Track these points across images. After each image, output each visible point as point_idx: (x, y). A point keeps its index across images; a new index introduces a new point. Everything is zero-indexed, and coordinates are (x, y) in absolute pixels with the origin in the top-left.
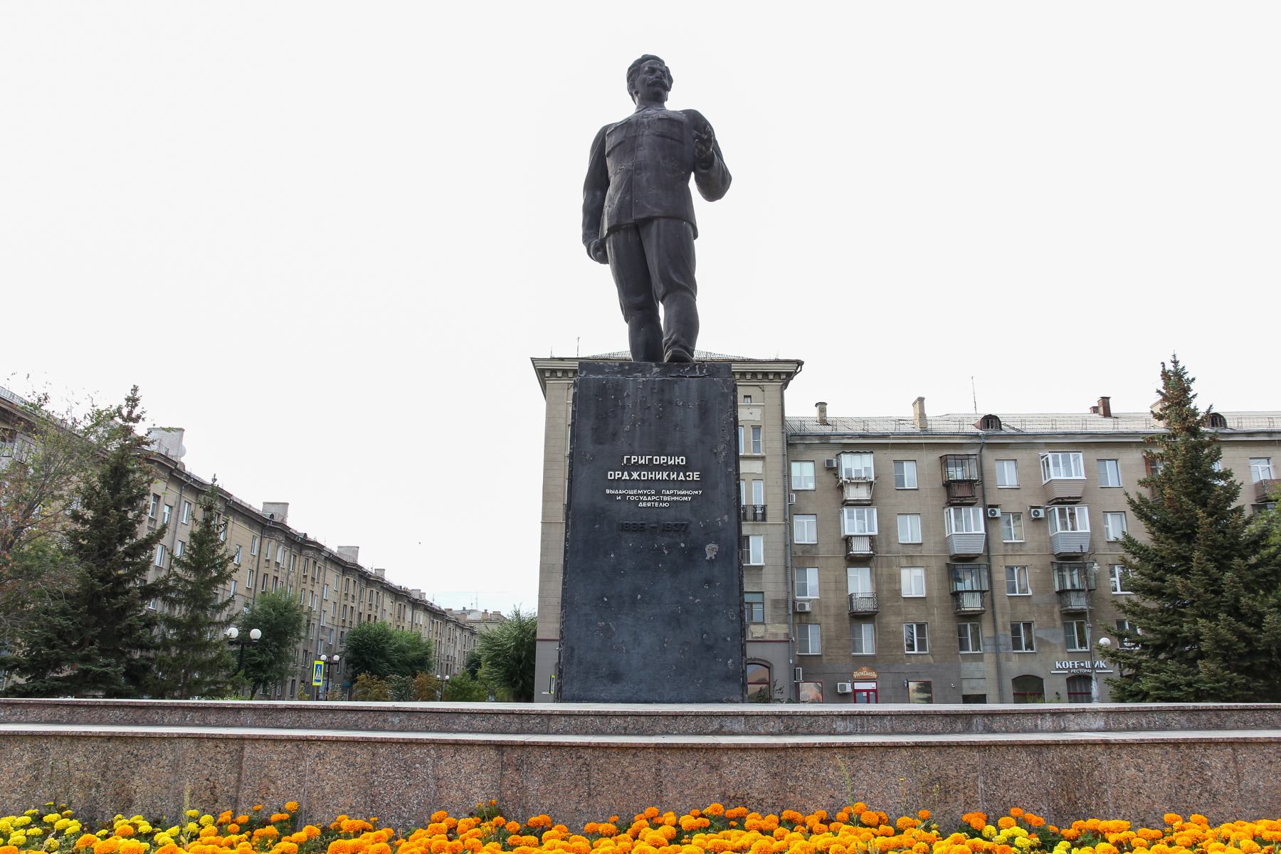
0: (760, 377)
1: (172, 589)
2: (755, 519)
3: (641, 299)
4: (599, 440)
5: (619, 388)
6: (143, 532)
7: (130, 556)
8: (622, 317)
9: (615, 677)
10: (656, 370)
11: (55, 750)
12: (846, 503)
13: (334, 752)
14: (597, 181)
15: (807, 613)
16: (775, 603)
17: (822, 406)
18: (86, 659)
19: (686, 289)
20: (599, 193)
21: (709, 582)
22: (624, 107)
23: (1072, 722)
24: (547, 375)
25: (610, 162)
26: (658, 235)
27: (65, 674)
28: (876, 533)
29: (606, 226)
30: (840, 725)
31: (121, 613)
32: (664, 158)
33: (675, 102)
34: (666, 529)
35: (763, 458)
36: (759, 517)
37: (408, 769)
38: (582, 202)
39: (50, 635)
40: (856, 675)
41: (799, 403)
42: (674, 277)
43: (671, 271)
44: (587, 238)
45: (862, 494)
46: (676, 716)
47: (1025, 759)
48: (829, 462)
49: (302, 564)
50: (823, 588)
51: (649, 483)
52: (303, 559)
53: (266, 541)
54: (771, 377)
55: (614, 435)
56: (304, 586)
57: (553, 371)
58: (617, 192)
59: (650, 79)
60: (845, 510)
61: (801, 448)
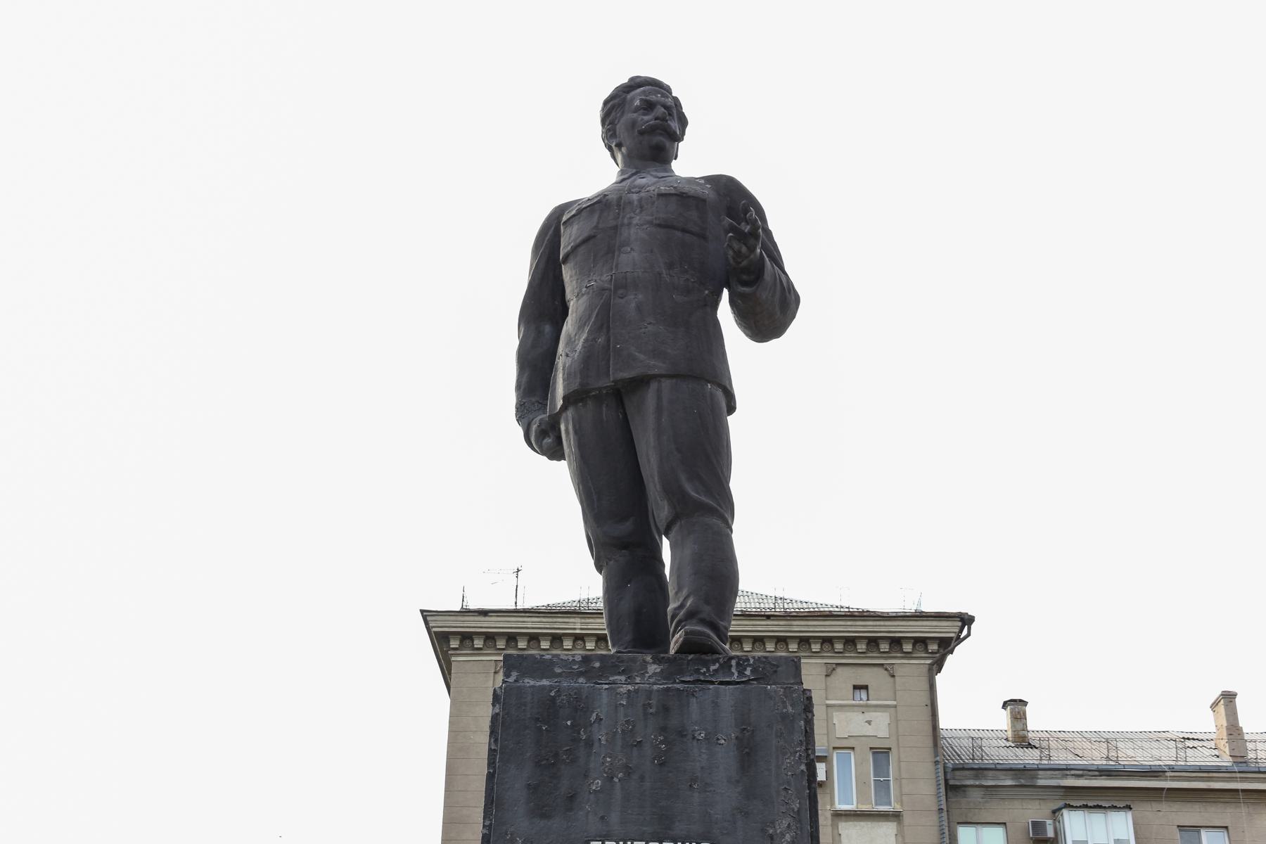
0: (884, 647)
3: (627, 527)
4: (541, 811)
5: (580, 706)
8: (590, 561)
10: (653, 668)
14: (543, 307)
17: (1016, 707)
19: (712, 511)
20: (547, 328)
22: (596, 171)
24: (454, 643)
25: (568, 274)
26: (659, 409)
29: (560, 390)
32: (670, 266)
33: (692, 161)
35: (896, 816)
38: (515, 343)
41: (968, 700)
42: (689, 489)
43: (683, 478)
44: (523, 413)
48: (1038, 826)
54: (908, 647)
55: (572, 798)
57: (466, 638)
58: (580, 327)
59: (643, 120)
61: (976, 795)
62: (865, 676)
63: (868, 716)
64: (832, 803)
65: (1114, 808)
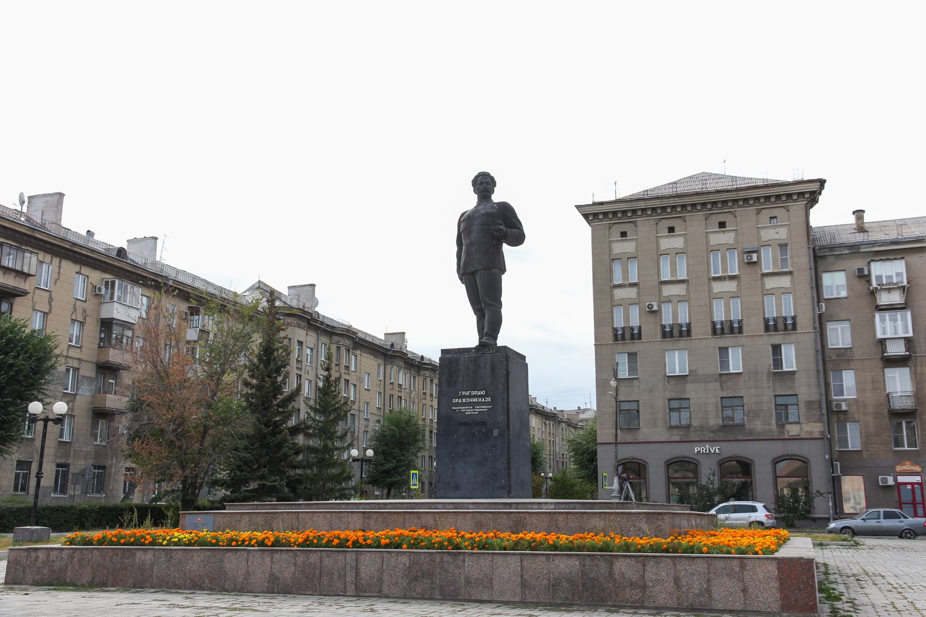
1: (309, 427)
2: (786, 329)
6: (287, 390)
7: (281, 407)
9: (457, 488)
11: (254, 517)
12: (879, 309)
13: (321, 516)
15: (845, 412)
16: (809, 404)
17: (859, 214)
18: (262, 477)
21: (495, 446)
22: (471, 201)
23: (544, 506)
27: (251, 487)
28: (910, 334)
30: (471, 506)
31: (280, 446)
33: (496, 197)
34: (477, 424)
35: (790, 273)
36: (790, 327)
37: (340, 519)
39: (239, 463)
40: (899, 468)
41: (827, 215)
45: (896, 298)
46: (422, 503)
47: (505, 516)
48: (860, 270)
49: (421, 383)
50: (860, 386)
51: (469, 404)
52: (421, 379)
53: (389, 367)
56: (424, 402)
59: (484, 184)
60: (877, 316)
61: (831, 259)
62: (775, 212)
63: (777, 230)
64: (761, 270)
65: (895, 259)
